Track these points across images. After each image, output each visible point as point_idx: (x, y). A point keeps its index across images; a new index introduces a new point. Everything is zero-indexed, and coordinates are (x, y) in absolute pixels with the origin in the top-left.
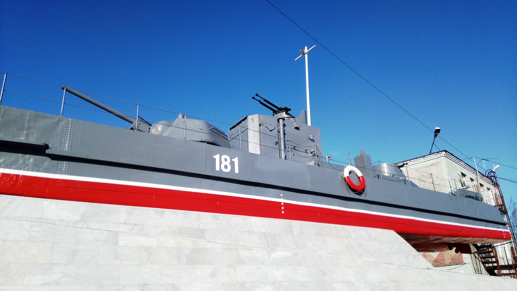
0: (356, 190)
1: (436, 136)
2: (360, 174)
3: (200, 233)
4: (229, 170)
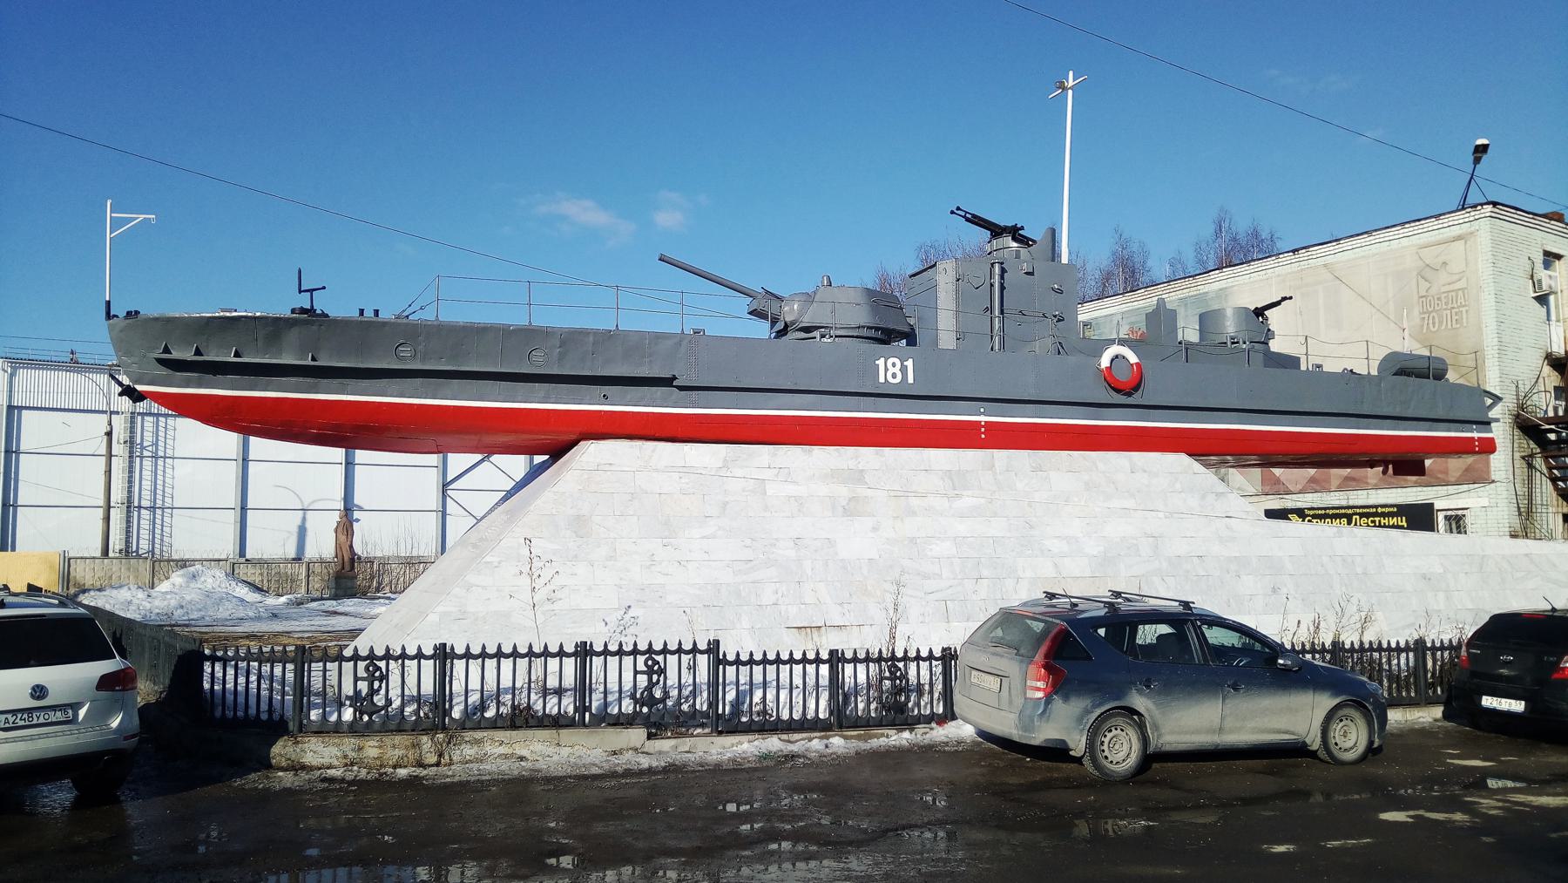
0: (1126, 388)
1: (1477, 161)
3: (859, 476)
4: (898, 379)
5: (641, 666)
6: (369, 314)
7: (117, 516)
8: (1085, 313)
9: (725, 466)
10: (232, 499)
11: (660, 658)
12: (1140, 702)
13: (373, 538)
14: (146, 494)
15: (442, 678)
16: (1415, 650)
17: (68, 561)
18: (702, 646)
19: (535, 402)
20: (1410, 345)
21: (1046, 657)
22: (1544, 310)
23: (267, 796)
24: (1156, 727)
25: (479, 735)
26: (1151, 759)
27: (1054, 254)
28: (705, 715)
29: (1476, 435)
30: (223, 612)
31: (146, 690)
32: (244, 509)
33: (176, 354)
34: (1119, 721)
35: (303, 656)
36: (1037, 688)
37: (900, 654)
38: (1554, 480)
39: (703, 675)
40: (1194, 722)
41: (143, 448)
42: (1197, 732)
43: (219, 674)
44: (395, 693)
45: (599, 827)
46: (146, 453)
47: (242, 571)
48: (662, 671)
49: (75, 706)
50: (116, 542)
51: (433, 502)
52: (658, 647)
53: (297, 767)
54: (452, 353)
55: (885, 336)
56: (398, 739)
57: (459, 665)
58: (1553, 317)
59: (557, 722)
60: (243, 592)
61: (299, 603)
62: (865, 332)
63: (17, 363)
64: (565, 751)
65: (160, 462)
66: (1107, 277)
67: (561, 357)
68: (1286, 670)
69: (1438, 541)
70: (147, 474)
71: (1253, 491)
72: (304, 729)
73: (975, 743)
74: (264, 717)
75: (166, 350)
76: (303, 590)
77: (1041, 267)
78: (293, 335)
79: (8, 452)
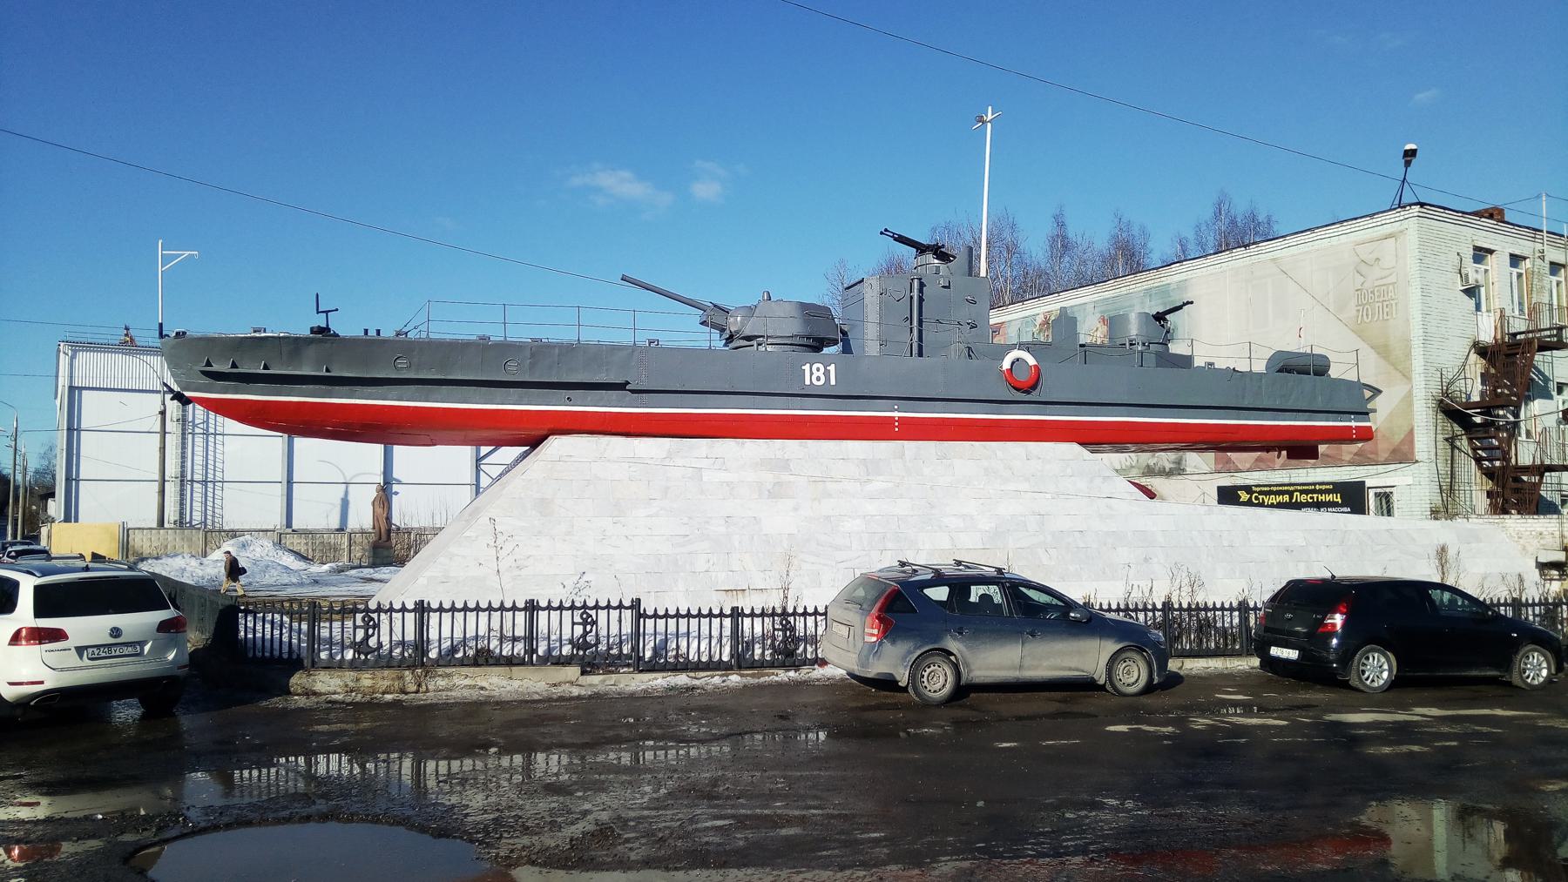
0: (1026, 388)
1: (1408, 164)
2: (1031, 361)
3: (784, 465)
5: (577, 619)
6: (372, 333)
7: (171, 490)
8: (995, 318)
9: (669, 456)
10: (279, 473)
11: (593, 613)
12: (953, 645)
13: (408, 510)
14: (198, 469)
15: (421, 626)
16: (1239, 609)
17: (126, 531)
18: (627, 603)
19: (515, 400)
20: (1293, 345)
21: (880, 610)
22: (1472, 302)
23: (285, 713)
24: (967, 665)
25: (448, 670)
26: (963, 691)
27: (971, 269)
28: (629, 657)
29: (1353, 424)
30: (270, 578)
31: (195, 638)
32: (290, 483)
33: (216, 367)
34: (937, 659)
35: (314, 612)
36: (872, 634)
37: (790, 611)
38: (1478, 460)
39: (627, 628)
40: (997, 660)
41: (194, 426)
42: (1001, 668)
43: (250, 625)
44: (385, 639)
45: (521, 731)
46: (197, 430)
47: (291, 541)
48: (594, 623)
49: (142, 644)
50: (171, 513)
51: (468, 477)
52: (591, 603)
53: (309, 693)
54: (440, 364)
55: (816, 345)
56: (386, 672)
57: (434, 617)
58: (1484, 308)
59: (511, 662)
60: (289, 560)
61: (340, 571)
62: (797, 341)
63: (78, 346)
64: (516, 684)
65: (211, 439)
66: (1109, 261)
67: (532, 366)
68: (1077, 621)
69: (1370, 522)
70: (199, 450)
71: (1207, 469)
72: (315, 665)
73: (842, 680)
74: (285, 656)
75: (209, 364)
76: (346, 559)
77: (960, 281)
78: (311, 351)
79: (70, 429)
